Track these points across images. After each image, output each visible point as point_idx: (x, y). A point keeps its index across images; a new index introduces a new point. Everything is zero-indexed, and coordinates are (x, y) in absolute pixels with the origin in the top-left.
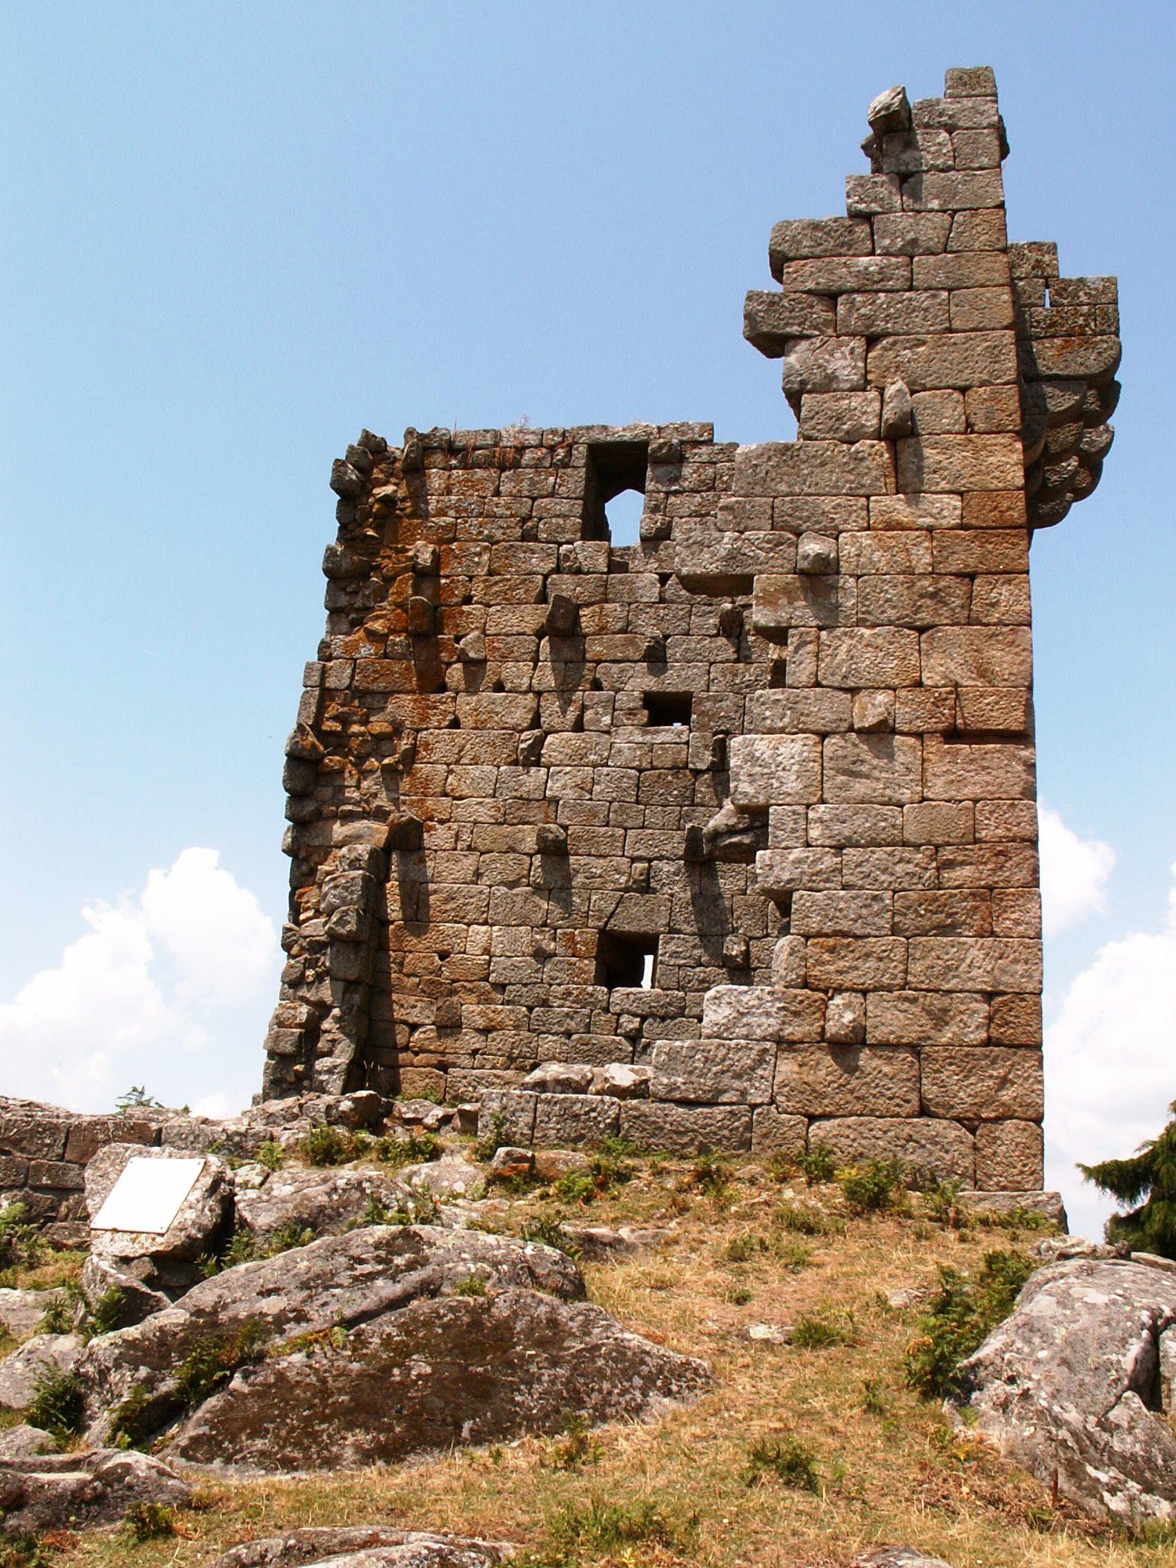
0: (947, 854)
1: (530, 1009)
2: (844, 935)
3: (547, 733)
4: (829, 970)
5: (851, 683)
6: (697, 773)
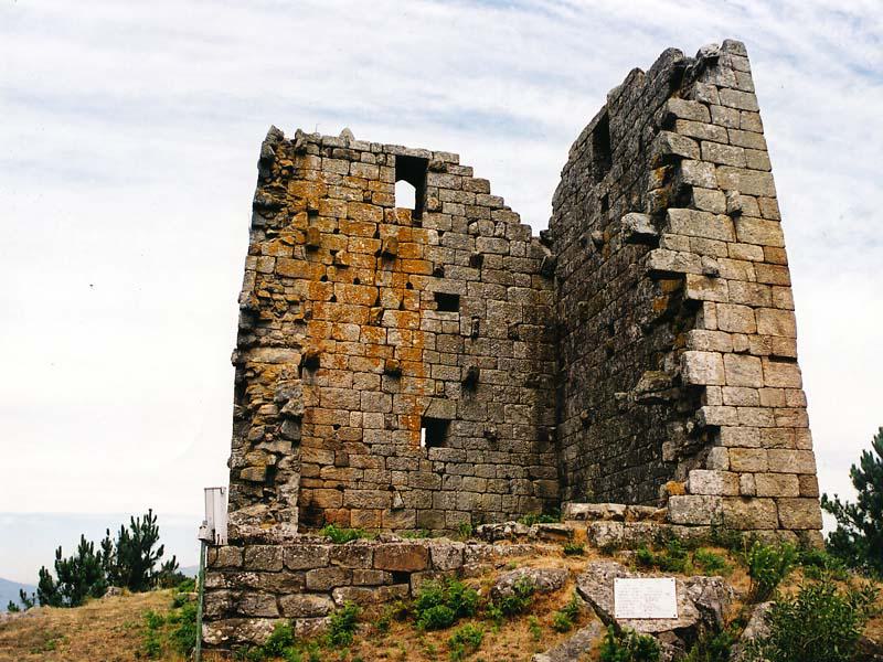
0: (777, 411)
1: (386, 457)
2: (743, 447)
3: (384, 309)
4: (738, 464)
5: (730, 330)
6: (465, 337)
